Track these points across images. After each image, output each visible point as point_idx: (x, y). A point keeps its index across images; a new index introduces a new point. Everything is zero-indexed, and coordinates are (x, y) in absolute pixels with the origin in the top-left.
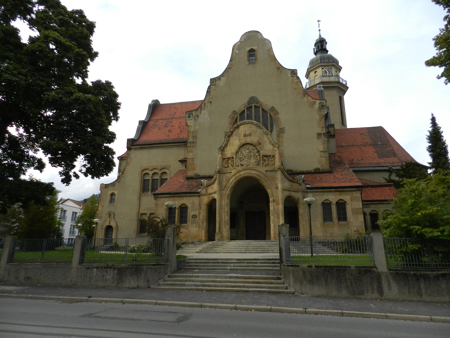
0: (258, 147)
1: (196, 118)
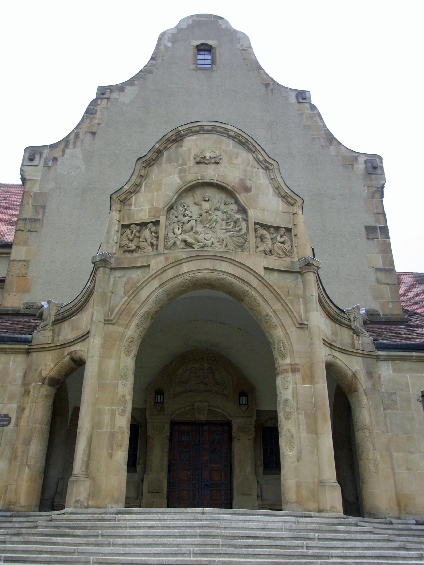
1: (50, 164)
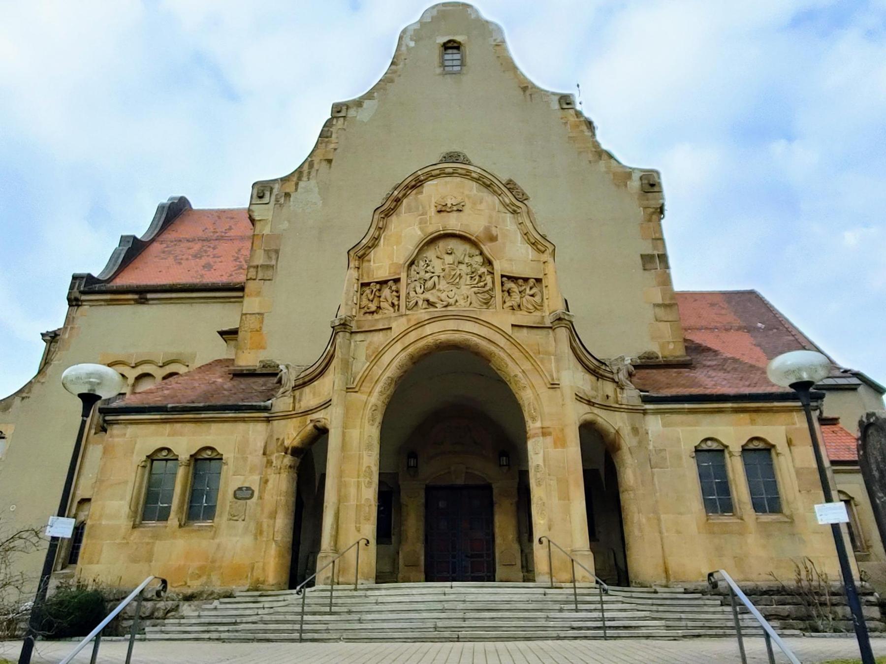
0: (486, 249)
1: (282, 201)
